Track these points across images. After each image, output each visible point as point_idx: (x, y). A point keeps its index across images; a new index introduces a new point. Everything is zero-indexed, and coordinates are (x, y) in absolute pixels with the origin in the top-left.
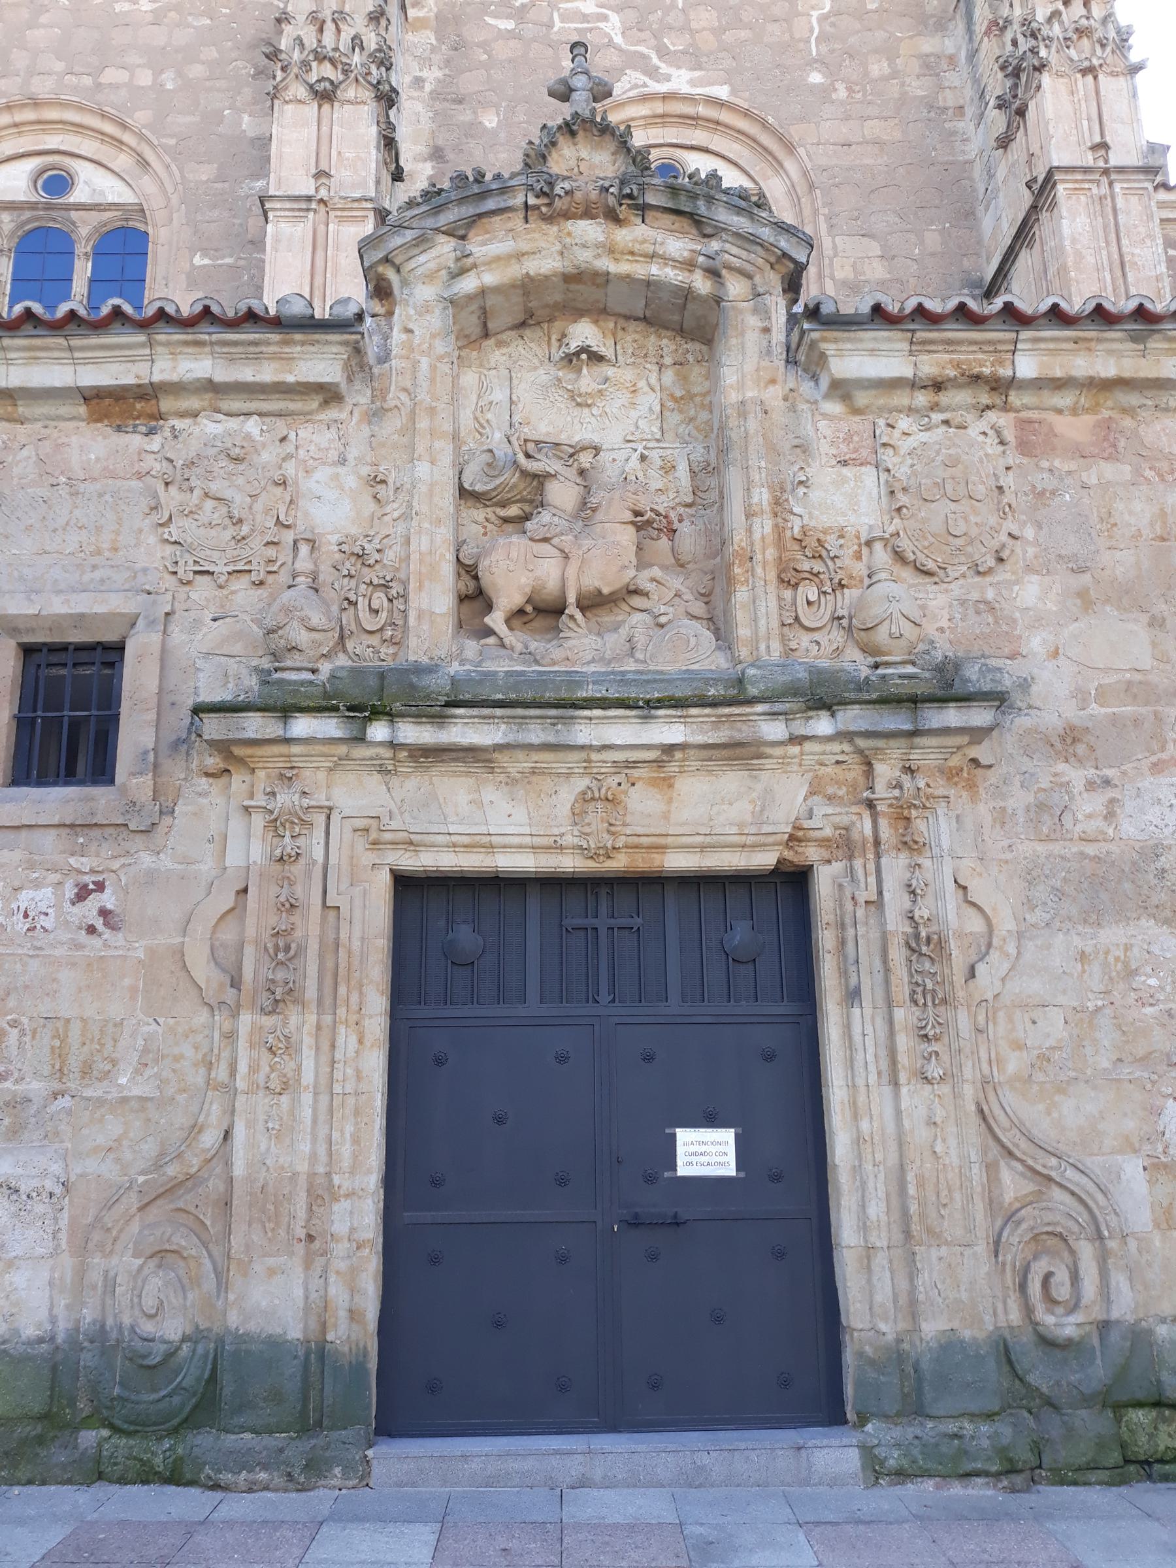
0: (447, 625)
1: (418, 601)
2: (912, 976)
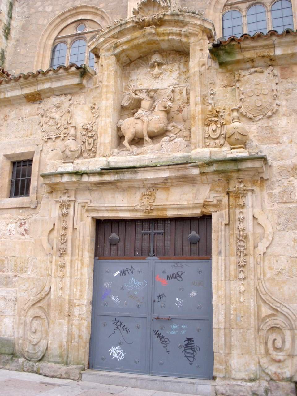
0: (109, 146)
1: (100, 140)
2: (237, 247)
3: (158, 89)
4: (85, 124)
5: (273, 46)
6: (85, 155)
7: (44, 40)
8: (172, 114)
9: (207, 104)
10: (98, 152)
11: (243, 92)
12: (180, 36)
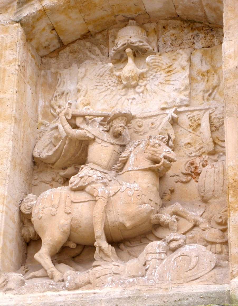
8: (170, 182)
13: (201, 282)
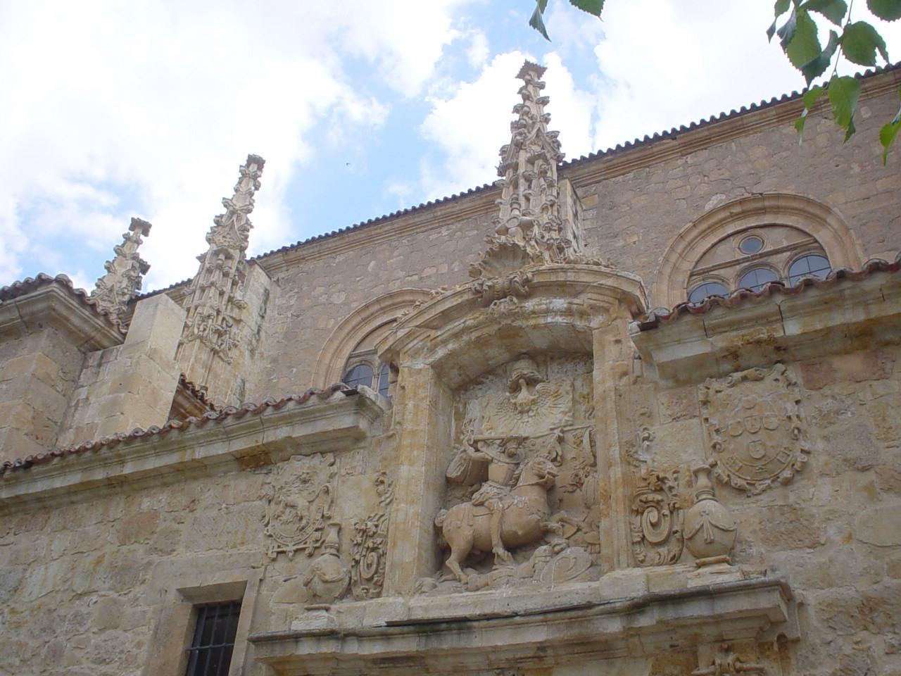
3: (526, 438)
4: (361, 520)
5: (781, 316)
6: (358, 591)
7: (327, 361)
8: (559, 493)
9: (634, 463)
10: (385, 585)
11: (717, 427)
12: (571, 315)
13: (519, 624)
